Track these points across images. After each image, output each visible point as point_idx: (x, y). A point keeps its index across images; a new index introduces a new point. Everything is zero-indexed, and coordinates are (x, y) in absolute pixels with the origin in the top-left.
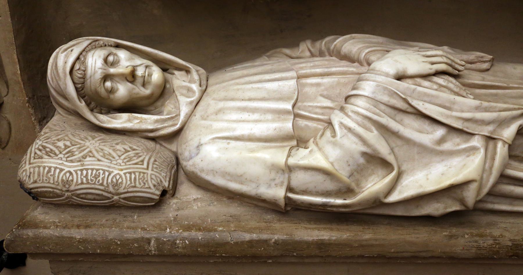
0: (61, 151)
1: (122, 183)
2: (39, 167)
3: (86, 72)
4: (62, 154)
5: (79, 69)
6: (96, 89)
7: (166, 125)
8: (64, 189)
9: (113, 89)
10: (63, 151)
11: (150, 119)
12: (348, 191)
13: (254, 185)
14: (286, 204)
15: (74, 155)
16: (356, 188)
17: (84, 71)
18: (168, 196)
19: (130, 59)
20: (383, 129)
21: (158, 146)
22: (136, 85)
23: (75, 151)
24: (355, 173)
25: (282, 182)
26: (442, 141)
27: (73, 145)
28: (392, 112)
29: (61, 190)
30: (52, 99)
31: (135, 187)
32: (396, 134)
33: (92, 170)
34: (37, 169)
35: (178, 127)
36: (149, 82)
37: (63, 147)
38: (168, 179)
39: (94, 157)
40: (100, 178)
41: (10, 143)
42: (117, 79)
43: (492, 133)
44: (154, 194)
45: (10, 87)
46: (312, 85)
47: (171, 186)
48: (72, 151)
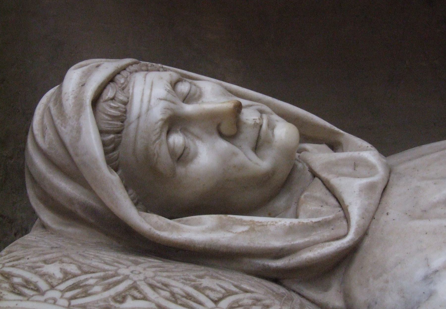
0: (55, 283)
3: (128, 107)
4: (56, 290)
5: (113, 99)
6: (147, 149)
9: (187, 151)
10: (59, 284)
11: (273, 225)
15: (90, 295)
17: (125, 104)
22: (240, 147)
23: (93, 286)
27: (86, 273)
30: (31, 192)
35: (352, 240)
36: (269, 142)
37: (59, 275)
39: (145, 298)
42: (196, 130)
48: (84, 284)
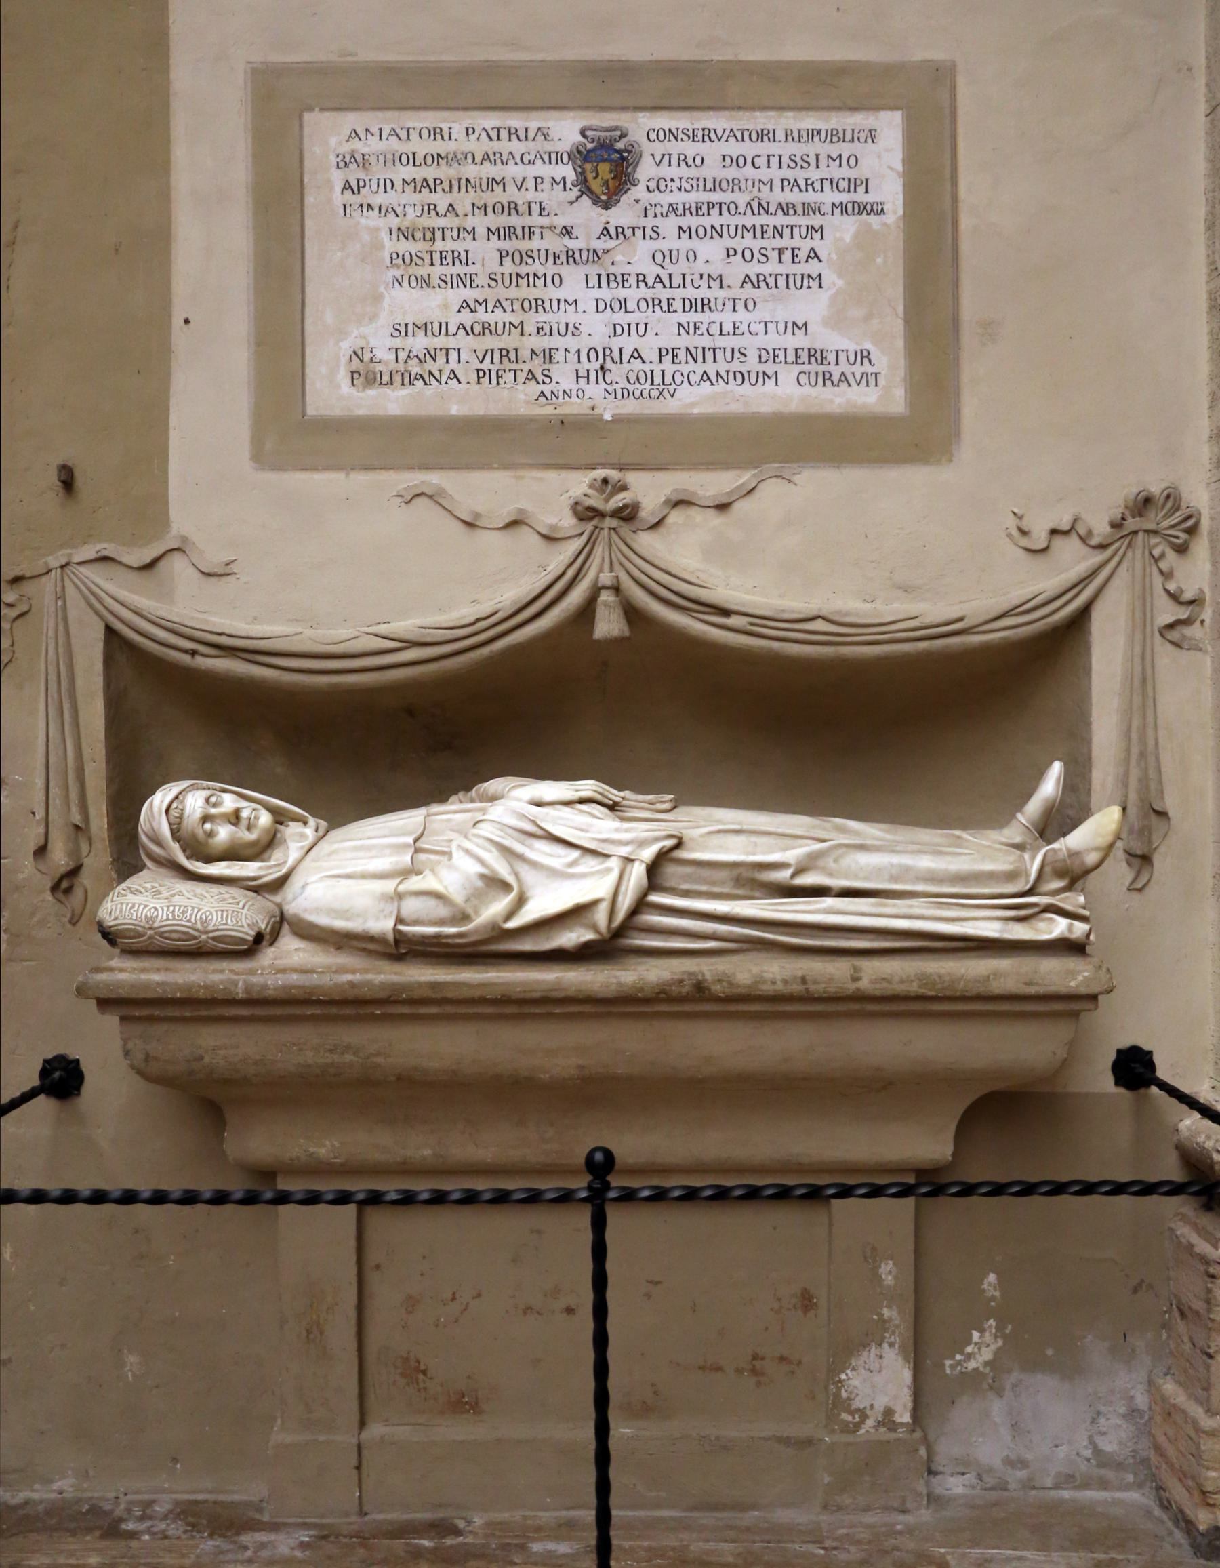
1: (211, 920)
2: (122, 904)
6: (193, 832)
7: (271, 871)
8: (147, 926)
12: (465, 918)
13: (360, 920)
14: (397, 941)
16: (472, 914)
18: (264, 943)
19: (235, 801)
20: (505, 851)
21: (259, 897)
24: (472, 899)
25: (391, 912)
26: (573, 864)
28: (522, 837)
29: (144, 927)
30: (141, 852)
31: (226, 924)
32: (521, 858)
33: (180, 906)
34: (119, 906)
36: (255, 826)
38: (265, 922)
40: (188, 915)
41: (84, 918)
43: (632, 853)
44: (247, 934)
45: (93, 846)
46: (442, 821)
47: (268, 930)
